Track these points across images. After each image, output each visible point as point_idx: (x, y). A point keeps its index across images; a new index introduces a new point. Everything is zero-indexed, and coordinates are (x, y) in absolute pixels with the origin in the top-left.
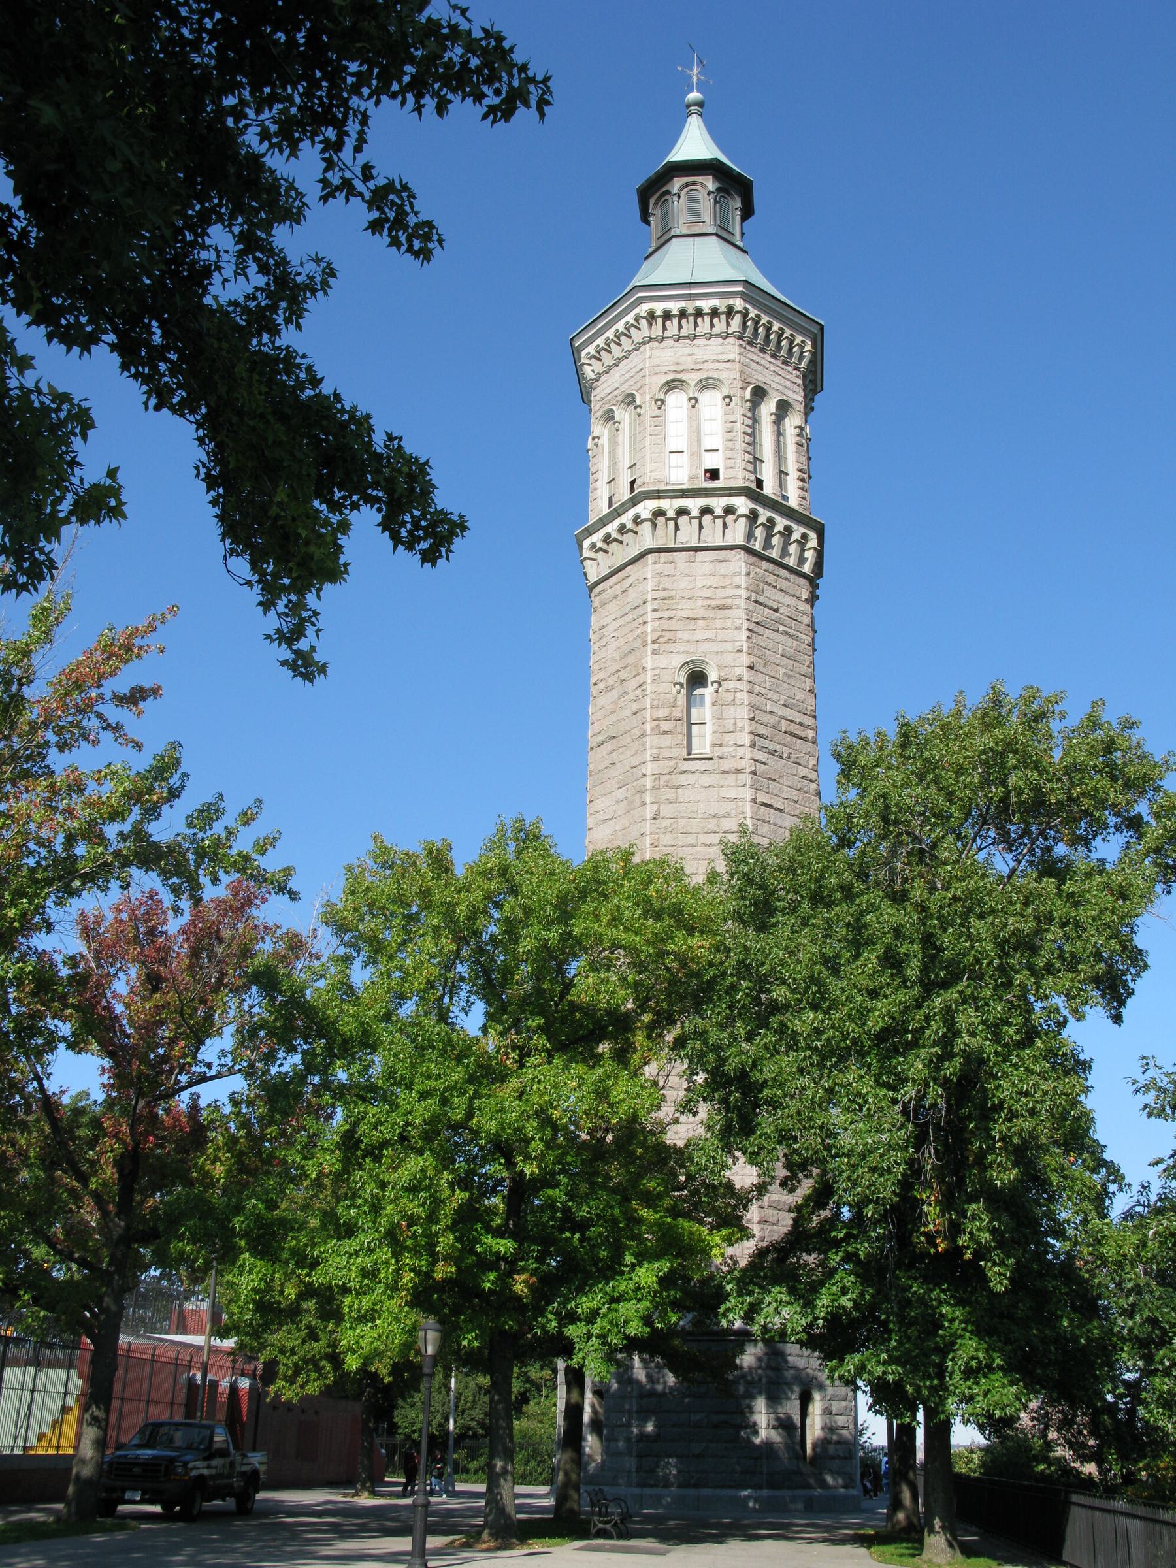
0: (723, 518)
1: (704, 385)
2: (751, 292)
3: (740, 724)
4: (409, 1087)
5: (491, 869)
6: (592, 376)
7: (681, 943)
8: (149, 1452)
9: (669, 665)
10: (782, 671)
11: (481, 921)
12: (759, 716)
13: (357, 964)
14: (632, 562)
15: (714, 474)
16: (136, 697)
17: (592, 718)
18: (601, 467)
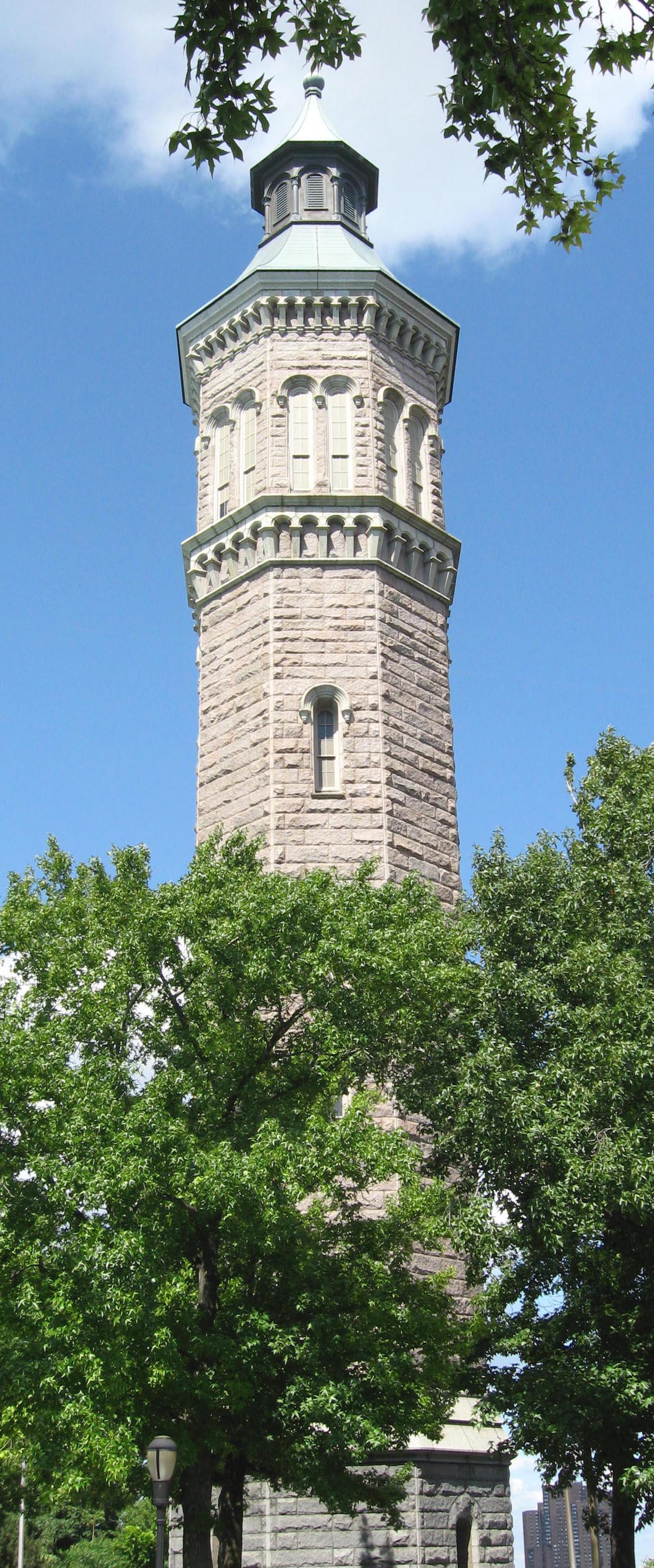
3: (375, 758)
12: (396, 750)
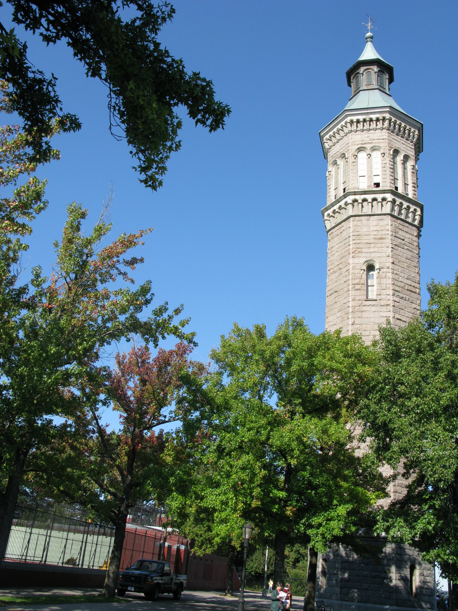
0: (381, 202)
1: (374, 149)
2: (393, 111)
3: (388, 286)
4: (244, 426)
5: (281, 336)
6: (328, 147)
7: (360, 369)
8: (138, 572)
9: (360, 262)
10: (406, 265)
11: (276, 359)
12: (396, 283)
13: (225, 375)
14: (344, 221)
15: (377, 185)
16: (133, 262)
17: (328, 284)
18: (332, 184)
